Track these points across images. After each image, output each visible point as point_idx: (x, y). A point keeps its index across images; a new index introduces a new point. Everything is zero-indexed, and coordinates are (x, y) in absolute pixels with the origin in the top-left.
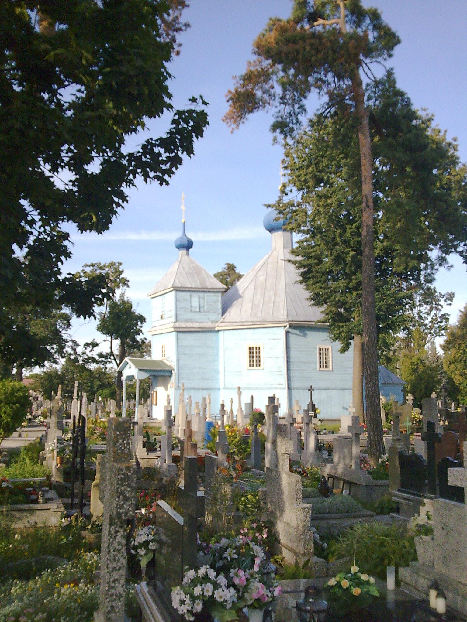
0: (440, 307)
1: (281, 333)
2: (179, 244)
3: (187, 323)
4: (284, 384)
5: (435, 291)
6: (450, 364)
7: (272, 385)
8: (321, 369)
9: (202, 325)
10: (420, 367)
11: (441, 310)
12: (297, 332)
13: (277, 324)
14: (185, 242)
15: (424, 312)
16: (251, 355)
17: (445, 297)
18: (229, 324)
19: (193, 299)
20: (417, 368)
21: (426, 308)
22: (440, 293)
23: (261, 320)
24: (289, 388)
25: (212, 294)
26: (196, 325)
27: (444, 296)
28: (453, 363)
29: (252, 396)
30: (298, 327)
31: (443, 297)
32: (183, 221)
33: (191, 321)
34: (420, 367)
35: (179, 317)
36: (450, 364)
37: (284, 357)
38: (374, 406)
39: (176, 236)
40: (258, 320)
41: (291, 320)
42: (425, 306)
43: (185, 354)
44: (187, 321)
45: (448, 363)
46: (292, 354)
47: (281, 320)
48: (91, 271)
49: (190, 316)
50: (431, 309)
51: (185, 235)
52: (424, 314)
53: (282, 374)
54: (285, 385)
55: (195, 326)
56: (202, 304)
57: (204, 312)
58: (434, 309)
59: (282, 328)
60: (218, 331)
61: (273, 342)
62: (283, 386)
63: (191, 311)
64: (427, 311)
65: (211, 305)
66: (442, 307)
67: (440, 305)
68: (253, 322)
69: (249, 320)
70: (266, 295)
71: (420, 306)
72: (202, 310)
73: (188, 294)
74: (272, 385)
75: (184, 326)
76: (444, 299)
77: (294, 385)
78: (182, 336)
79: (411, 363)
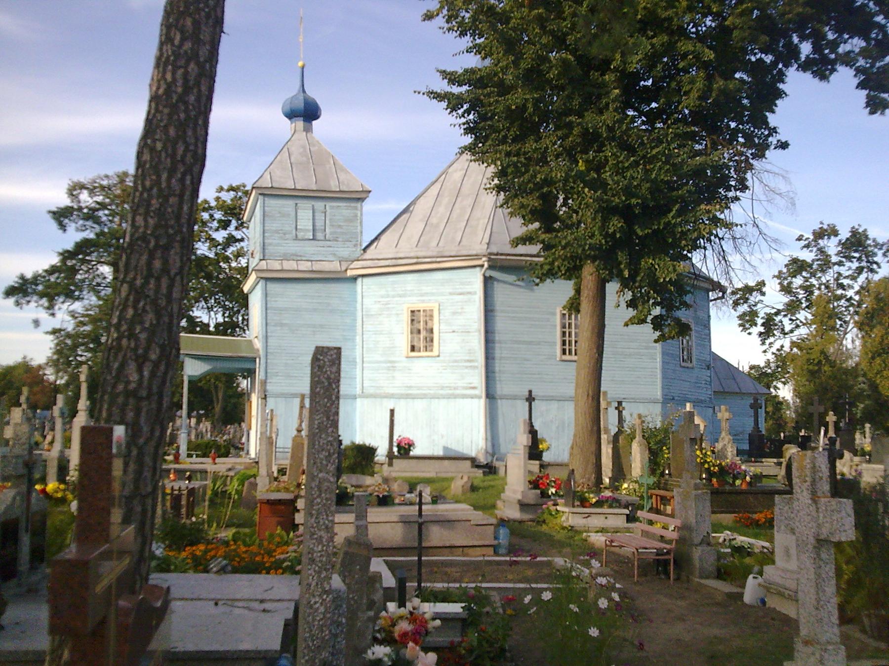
0: (875, 266)
1: (475, 281)
2: (288, 109)
3: (285, 262)
4: (479, 388)
5: (867, 238)
6: (873, 358)
7: (455, 388)
8: (567, 357)
9: (317, 267)
10: (826, 368)
11: (877, 273)
12: (511, 278)
13: (467, 262)
14: (300, 104)
15: (847, 273)
16: (416, 325)
17: (885, 248)
18: (369, 263)
19: (301, 213)
20: (820, 369)
21: (850, 268)
22: (874, 240)
23: (435, 254)
24: (490, 396)
25: (342, 204)
26: (305, 266)
27: (882, 245)
28: (880, 355)
29: (392, 412)
30: (499, 267)
31: (881, 249)
32: (300, 64)
33: (297, 258)
34: (826, 368)
35: (270, 250)
36: (873, 358)
37: (480, 331)
38: (114, 397)
39: (289, 91)
40: (430, 254)
41: (495, 251)
42: (848, 264)
43: (282, 325)
44: (286, 257)
45: (870, 355)
46: (500, 324)
47: (474, 252)
48: (232, 200)
49: (293, 247)
50: (860, 270)
51: (304, 91)
52: (845, 278)
53: (476, 367)
54: (481, 391)
55: (301, 268)
56: (319, 224)
57: (325, 240)
58: (865, 270)
59: (478, 269)
60: (354, 279)
61: (457, 301)
62: (476, 392)
63: (296, 238)
64: (850, 272)
65: (340, 226)
66: (879, 267)
67: (876, 263)
68: (418, 258)
69: (412, 255)
70: (457, 205)
71: (840, 264)
72: (320, 235)
73: (291, 203)
74: (455, 388)
75: (279, 268)
76: (882, 251)
77: (501, 389)
78: (273, 287)
79: (808, 360)
